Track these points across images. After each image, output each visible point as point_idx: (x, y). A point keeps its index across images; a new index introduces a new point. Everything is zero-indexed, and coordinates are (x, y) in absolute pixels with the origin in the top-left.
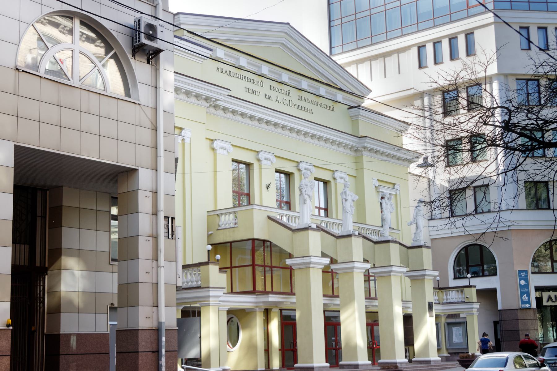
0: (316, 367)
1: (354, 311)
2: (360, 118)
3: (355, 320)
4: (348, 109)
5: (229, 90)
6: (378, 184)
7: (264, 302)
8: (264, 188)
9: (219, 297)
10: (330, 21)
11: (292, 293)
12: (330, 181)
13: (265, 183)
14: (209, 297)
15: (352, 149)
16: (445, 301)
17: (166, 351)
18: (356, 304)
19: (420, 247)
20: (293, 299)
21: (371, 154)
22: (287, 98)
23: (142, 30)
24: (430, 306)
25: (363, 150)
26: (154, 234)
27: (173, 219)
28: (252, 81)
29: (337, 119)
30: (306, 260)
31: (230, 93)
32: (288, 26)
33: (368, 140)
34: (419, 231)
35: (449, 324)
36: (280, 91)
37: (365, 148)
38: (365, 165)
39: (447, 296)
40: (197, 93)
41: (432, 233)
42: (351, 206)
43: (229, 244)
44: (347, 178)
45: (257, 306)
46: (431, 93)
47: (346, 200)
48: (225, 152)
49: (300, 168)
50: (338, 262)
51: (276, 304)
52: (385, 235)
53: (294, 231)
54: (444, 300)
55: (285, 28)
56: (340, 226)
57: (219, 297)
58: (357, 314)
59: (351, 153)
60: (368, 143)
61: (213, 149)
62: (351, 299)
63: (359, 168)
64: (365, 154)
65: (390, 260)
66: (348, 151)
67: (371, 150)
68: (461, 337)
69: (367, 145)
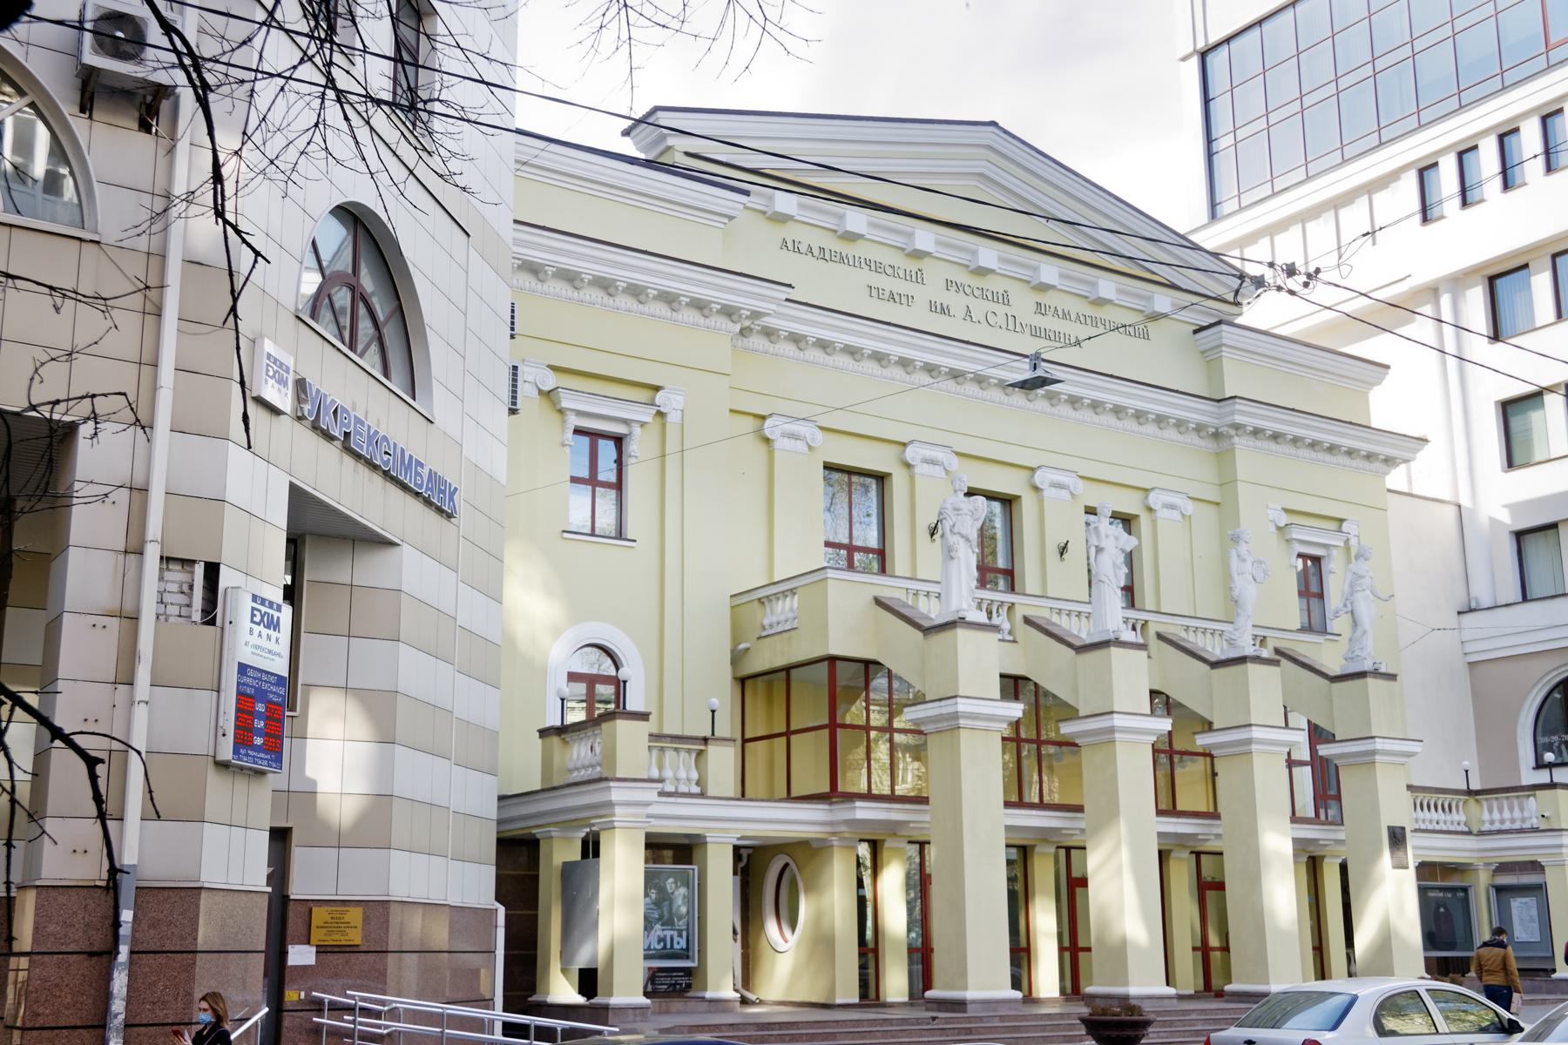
0: (974, 1002)
1: (1119, 844)
2: (1226, 352)
3: (1119, 871)
4: (1195, 332)
5: (790, 286)
6: (1284, 520)
7: (847, 822)
8: (1052, 552)
9: (647, 804)
10: (1209, 140)
11: (1215, 815)
12: (1136, 517)
13: (926, 518)
14: (610, 804)
15: (1203, 434)
16: (1486, 827)
17: (132, 952)
18: (1123, 826)
19: (1362, 675)
20: (1214, 827)
21: (1259, 443)
22: (1000, 309)
23: (88, 26)
24: (1397, 838)
25: (1233, 432)
26: (128, 608)
27: (212, 571)
28: (890, 271)
29: (1162, 358)
30: (945, 708)
31: (793, 295)
32: (992, 128)
33: (1239, 406)
34: (1359, 632)
35: (1500, 889)
36: (977, 293)
37: (1237, 427)
38: (1241, 473)
39: (1522, 809)
40: (630, 285)
41: (1469, 648)
42: (1114, 565)
43: (783, 674)
44: (1190, 508)
45: (834, 834)
46: (1458, 282)
47: (1099, 550)
48: (1064, 494)
49: (767, 433)
50: (1215, 726)
51: (1045, 834)
52: (1239, 643)
53: (928, 631)
54: (1483, 823)
55: (987, 135)
56: (1083, 619)
57: (647, 804)
58: (1125, 854)
59: (1202, 443)
60: (1242, 413)
61: (767, 440)
62: (1111, 812)
63: (1227, 481)
64: (1241, 443)
65: (1369, 723)
66: (1193, 438)
67: (1256, 432)
68: (1536, 925)
69: (1238, 419)
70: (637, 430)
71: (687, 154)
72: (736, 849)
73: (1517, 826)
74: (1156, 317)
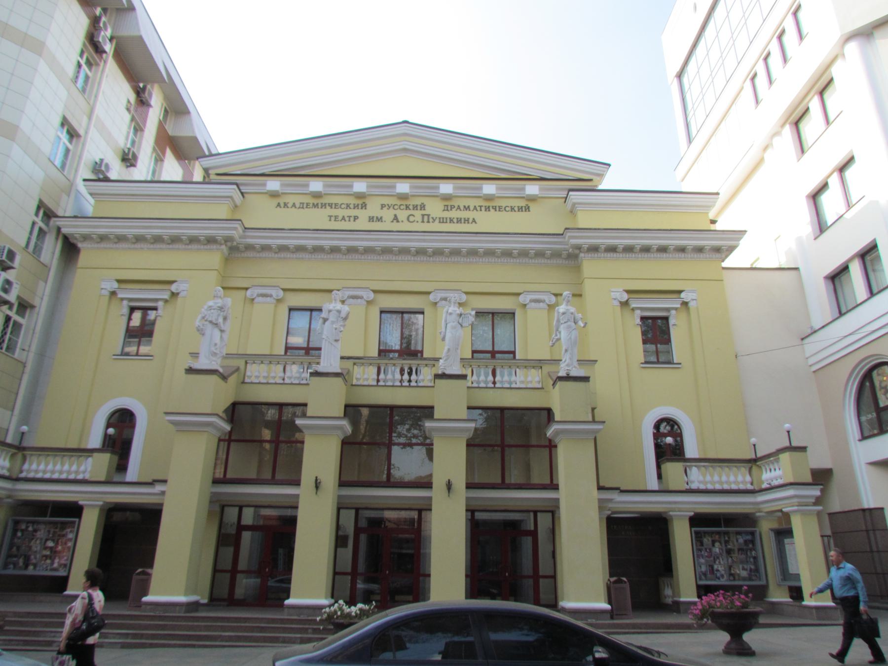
6: (625, 296)
70: (673, 312)
71: (218, 174)
72: (882, 509)
73: (64, 476)
74: (532, 199)
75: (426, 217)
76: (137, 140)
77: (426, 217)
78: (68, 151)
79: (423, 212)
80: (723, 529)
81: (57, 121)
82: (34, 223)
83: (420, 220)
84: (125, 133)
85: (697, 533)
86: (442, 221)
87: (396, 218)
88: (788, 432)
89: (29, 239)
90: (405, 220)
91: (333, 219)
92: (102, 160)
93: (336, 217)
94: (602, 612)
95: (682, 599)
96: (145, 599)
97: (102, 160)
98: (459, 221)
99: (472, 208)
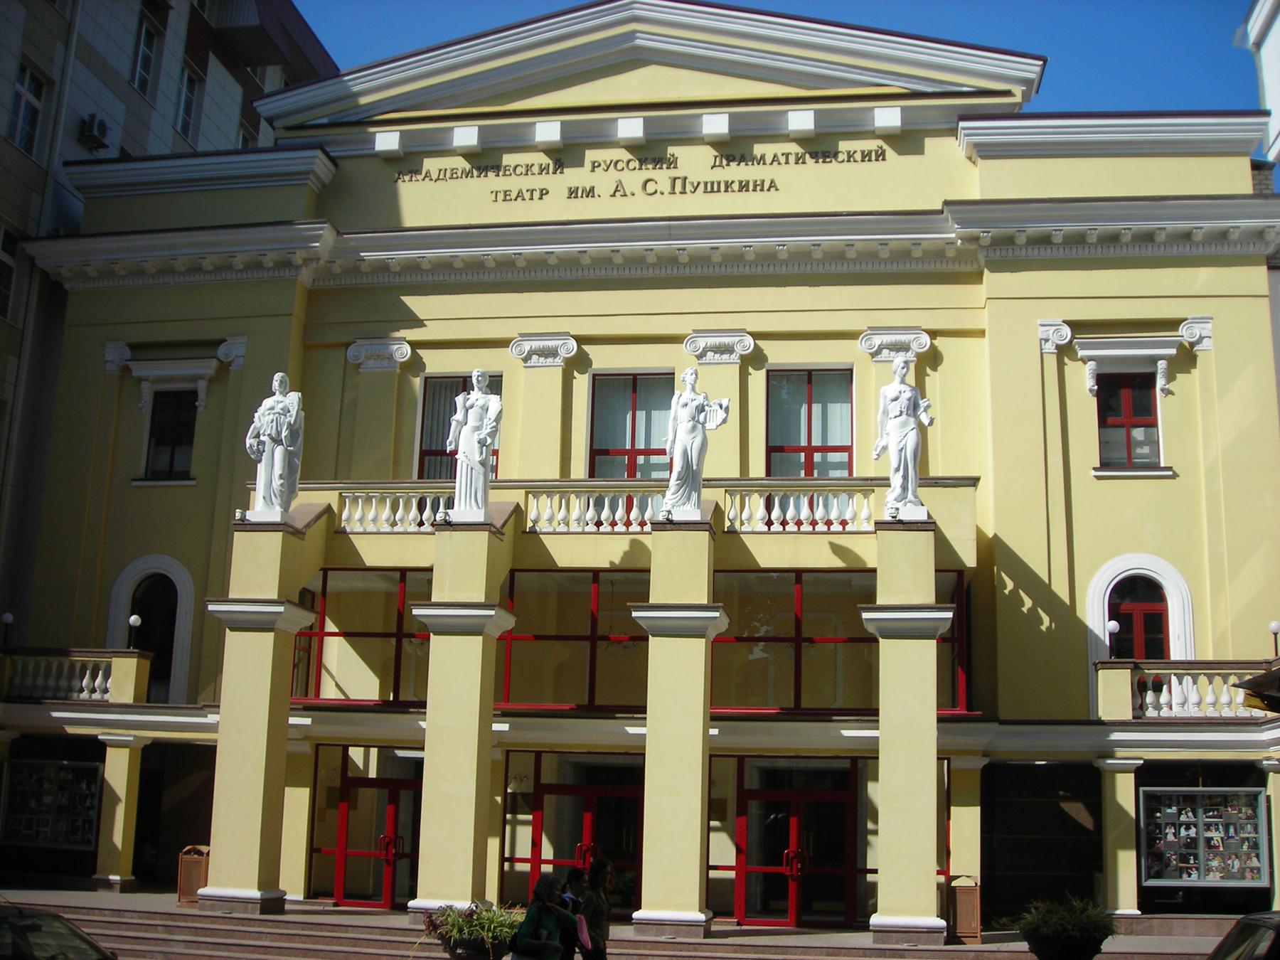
75: (679, 183)
76: (153, 56)
77: (679, 183)
78: (33, 112)
79: (673, 173)
80: (1201, 789)
81: (12, 66)
82: (18, 96)
83: (668, 189)
84: (129, 47)
85: (1148, 796)
86: (712, 188)
87: (618, 190)
88: (1276, 634)
89: (13, 126)
90: (638, 191)
91: (501, 196)
92: (93, 117)
93: (506, 193)
94: (931, 931)
95: (1118, 912)
96: (201, 891)
97: (93, 117)
98: (744, 187)
99: (769, 159)
